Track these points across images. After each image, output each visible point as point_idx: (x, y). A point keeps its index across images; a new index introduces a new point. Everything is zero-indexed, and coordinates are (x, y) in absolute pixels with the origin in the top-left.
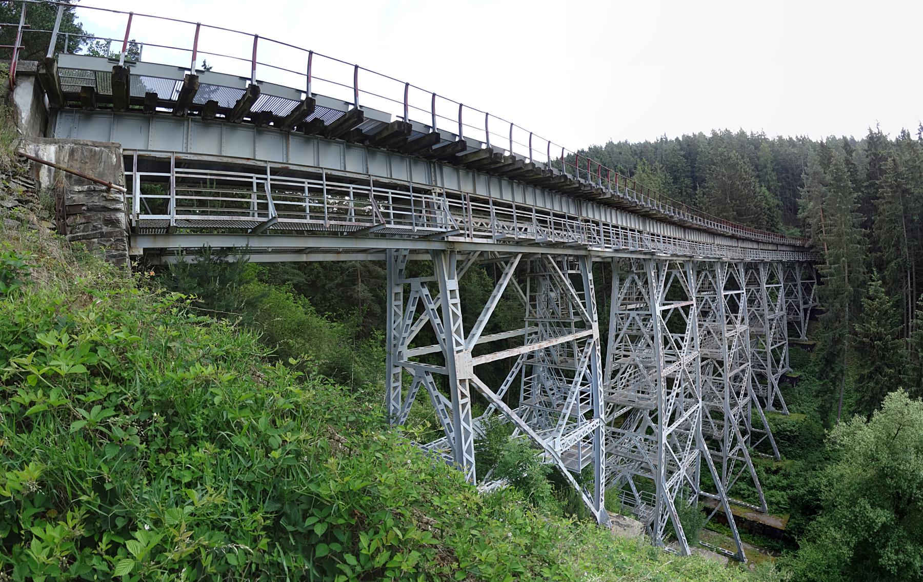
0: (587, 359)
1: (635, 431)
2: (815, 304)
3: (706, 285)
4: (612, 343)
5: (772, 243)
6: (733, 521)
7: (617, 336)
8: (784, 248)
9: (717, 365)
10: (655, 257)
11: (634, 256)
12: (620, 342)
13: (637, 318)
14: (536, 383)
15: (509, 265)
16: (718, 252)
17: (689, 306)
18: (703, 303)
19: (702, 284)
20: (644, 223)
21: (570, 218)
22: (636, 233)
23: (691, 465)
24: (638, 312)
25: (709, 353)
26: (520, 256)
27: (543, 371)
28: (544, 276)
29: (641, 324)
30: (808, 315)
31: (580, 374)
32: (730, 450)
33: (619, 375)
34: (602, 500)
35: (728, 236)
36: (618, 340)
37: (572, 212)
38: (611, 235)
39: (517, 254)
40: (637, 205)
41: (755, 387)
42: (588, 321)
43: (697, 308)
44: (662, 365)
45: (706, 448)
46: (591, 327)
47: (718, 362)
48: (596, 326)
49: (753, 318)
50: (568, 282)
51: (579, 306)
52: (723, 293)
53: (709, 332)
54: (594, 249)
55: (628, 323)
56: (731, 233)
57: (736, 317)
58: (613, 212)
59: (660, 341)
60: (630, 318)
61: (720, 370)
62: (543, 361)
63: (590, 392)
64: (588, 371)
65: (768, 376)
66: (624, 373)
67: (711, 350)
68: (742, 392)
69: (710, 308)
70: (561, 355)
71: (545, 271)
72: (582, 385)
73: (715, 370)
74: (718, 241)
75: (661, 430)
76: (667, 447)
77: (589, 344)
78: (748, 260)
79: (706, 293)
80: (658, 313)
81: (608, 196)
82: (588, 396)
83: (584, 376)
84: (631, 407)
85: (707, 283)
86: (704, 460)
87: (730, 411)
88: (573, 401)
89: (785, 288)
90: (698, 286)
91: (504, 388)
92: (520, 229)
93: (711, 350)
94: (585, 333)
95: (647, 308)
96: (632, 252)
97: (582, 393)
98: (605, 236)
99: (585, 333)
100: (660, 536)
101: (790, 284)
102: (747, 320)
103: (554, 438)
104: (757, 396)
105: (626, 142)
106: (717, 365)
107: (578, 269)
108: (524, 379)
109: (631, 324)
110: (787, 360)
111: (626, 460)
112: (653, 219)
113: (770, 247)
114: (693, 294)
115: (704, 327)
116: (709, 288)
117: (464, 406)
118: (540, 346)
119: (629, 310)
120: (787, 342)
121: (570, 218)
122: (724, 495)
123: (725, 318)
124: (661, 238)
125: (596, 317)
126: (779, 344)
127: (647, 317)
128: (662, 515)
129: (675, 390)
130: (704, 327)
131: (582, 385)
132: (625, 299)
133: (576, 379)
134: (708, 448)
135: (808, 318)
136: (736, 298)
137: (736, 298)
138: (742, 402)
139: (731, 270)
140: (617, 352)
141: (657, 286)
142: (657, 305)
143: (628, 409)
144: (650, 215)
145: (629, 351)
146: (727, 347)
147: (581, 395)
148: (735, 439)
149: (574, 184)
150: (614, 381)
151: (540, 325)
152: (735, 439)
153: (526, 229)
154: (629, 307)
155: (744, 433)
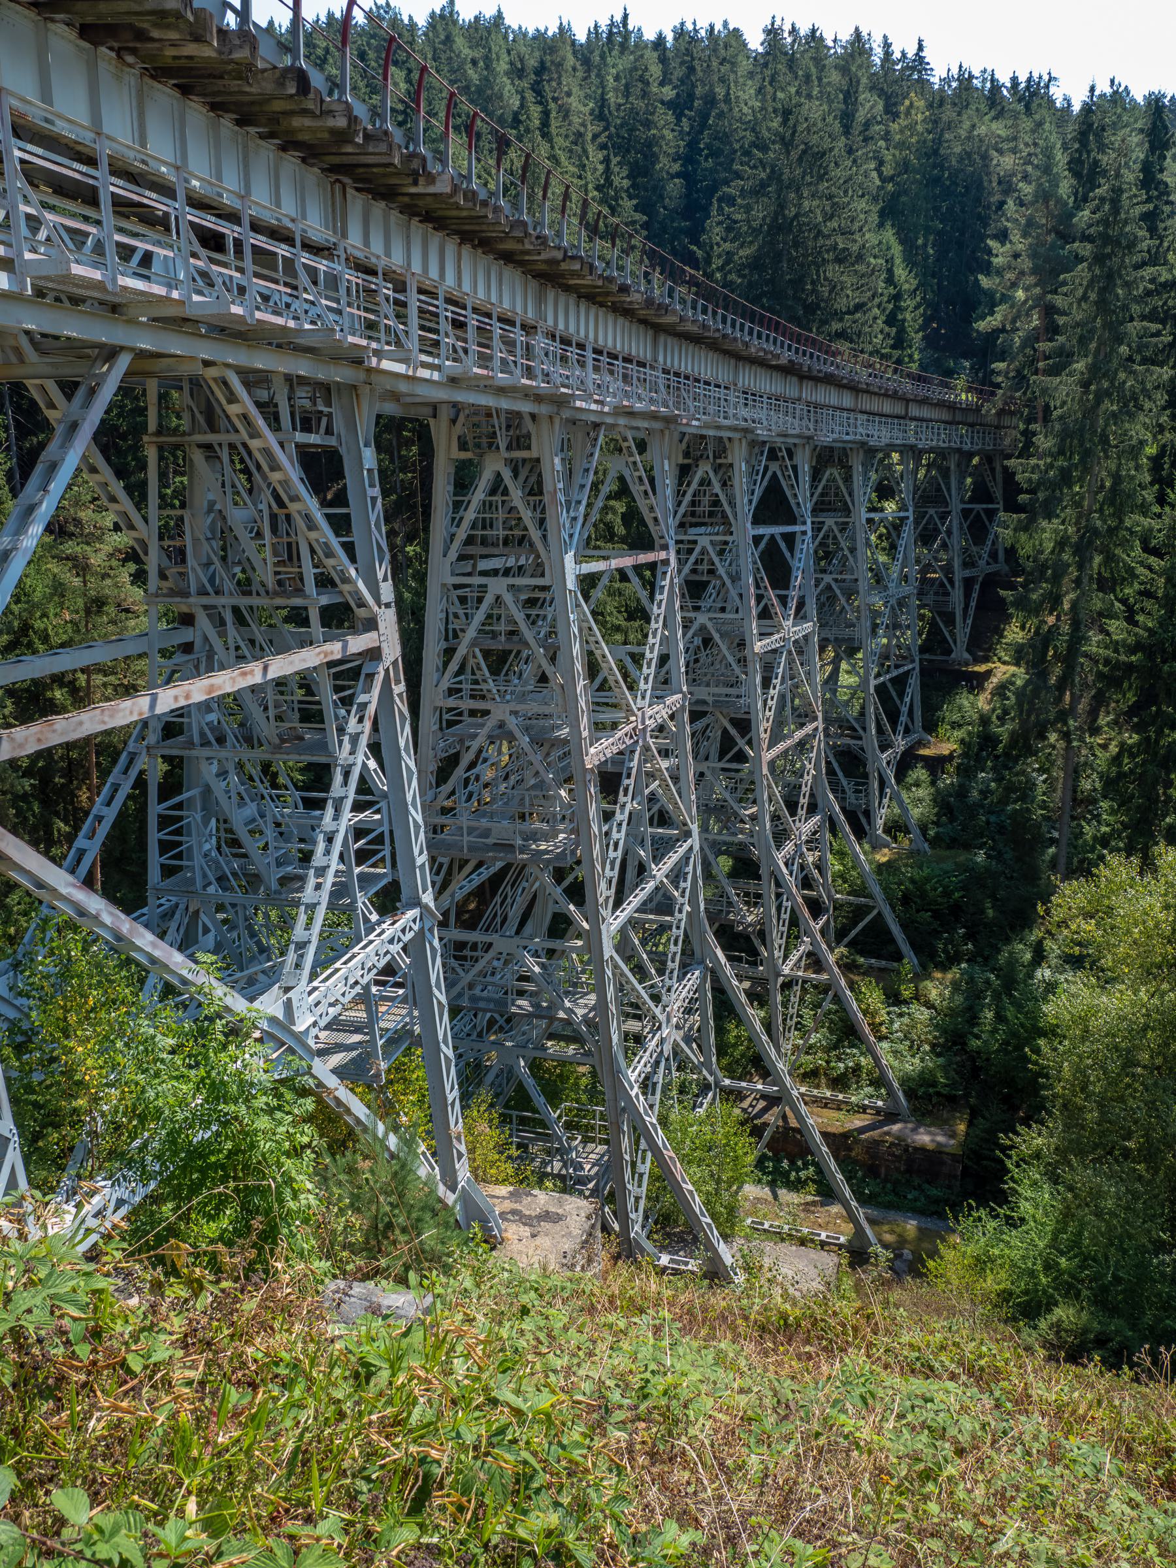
0: (368, 725)
1: (518, 932)
2: (993, 568)
3: (705, 507)
4: (436, 676)
5: (894, 396)
6: (825, 1149)
7: (449, 652)
8: (925, 412)
9: (733, 732)
10: (566, 414)
11: (505, 404)
12: (458, 674)
13: (508, 598)
14: (198, 817)
15: (81, 392)
16: (744, 412)
17: (652, 566)
18: (692, 559)
19: (693, 503)
20: (540, 300)
21: (308, 247)
22: (517, 330)
23: (688, 1011)
24: (510, 581)
25: (710, 699)
26: (124, 362)
27: (223, 774)
28: (208, 447)
29: (519, 616)
30: (975, 595)
31: (347, 775)
32: (786, 957)
33: (459, 773)
34: (460, 1155)
35: (778, 368)
36: (454, 666)
37: (315, 227)
38: (442, 320)
39: (111, 353)
40: (527, 234)
41: (836, 787)
42: (362, 604)
43: (679, 571)
44: (585, 734)
45: (722, 959)
46: (371, 624)
47: (735, 722)
48: (388, 620)
49: (827, 601)
50: (292, 472)
51: (330, 554)
52: (752, 531)
53: (707, 641)
54: (386, 365)
55: (480, 616)
56: (786, 356)
57: (784, 600)
58: (451, 247)
59: (578, 666)
60: (489, 599)
61: (741, 743)
62: (221, 740)
63: (385, 828)
64: (372, 764)
65: (869, 755)
66: (472, 765)
67: (716, 690)
68: (804, 801)
69: (711, 572)
70: (279, 718)
71: (213, 428)
72: (358, 807)
73: (727, 743)
74: (749, 378)
75: (596, 920)
76: (616, 966)
77: (371, 676)
78: (826, 438)
79: (702, 530)
80: (571, 583)
81: (442, 187)
82: (379, 840)
83: (362, 779)
84: (499, 865)
85: (706, 500)
86: (720, 991)
87: (776, 854)
88: (335, 865)
89: (917, 522)
90: (682, 510)
91: (91, 844)
92: (126, 252)
93: (716, 690)
94: (358, 643)
95: (539, 570)
96: (501, 391)
97: (359, 832)
98: (422, 328)
99: (358, 643)
100: (637, 1228)
101: (932, 511)
102: (811, 608)
103: (287, 990)
104: (843, 809)
105: (499, 16)
106: (733, 732)
107: (329, 431)
108: (155, 809)
109: (489, 616)
110: (918, 713)
111: (501, 1021)
112: (567, 289)
113: (887, 407)
114: (667, 527)
115: (695, 627)
116: (711, 514)
117: (637, 1096)
118: (211, 688)
119: (484, 573)
120: (917, 665)
121: (308, 247)
122: (788, 1081)
123: (753, 602)
124: (590, 355)
125: (387, 591)
126: (895, 673)
127: (537, 594)
128: (634, 1164)
129: (628, 804)
130: (695, 627)
131: (358, 807)
132: (470, 541)
133: (337, 789)
134: (730, 958)
135: (973, 604)
136: (783, 545)
137: (783, 545)
138: (805, 827)
139: (774, 467)
140: (451, 702)
141: (568, 503)
142: (569, 558)
143: (493, 870)
144: (562, 276)
145: (483, 697)
146: (758, 680)
147: (356, 841)
148: (794, 922)
149: (330, 113)
150: (446, 788)
151: (202, 621)
152: (794, 922)
153: (147, 259)
154: (483, 565)
155: (816, 908)
